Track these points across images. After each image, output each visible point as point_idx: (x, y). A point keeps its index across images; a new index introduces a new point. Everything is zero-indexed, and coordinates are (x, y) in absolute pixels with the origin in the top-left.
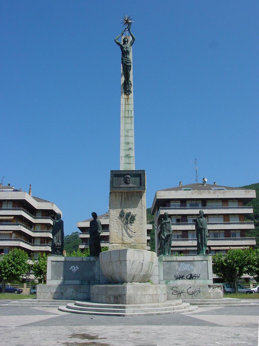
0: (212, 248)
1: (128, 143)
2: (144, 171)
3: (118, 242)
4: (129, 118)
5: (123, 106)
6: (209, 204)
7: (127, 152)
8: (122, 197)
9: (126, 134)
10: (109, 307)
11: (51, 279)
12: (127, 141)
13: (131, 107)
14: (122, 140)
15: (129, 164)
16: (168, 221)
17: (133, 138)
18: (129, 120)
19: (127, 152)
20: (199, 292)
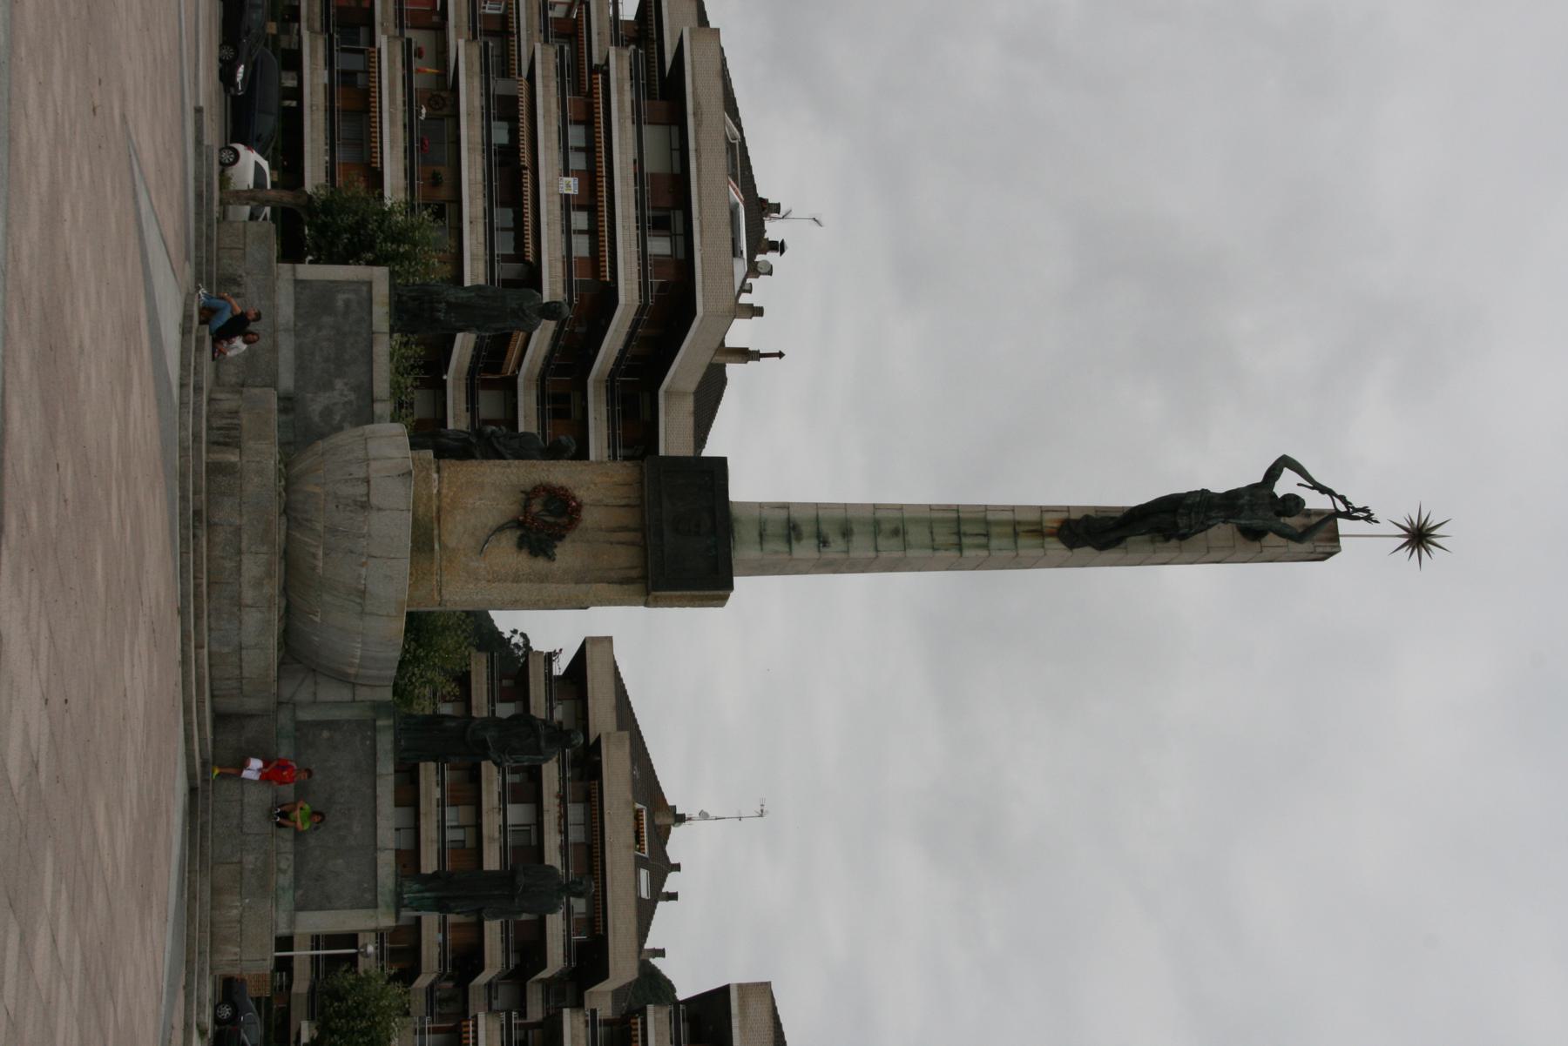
2: (610, 639)
3: (444, 491)
4: (954, 539)
11: (297, 282)
12: (856, 529)
15: (761, 536)
16: (543, 744)
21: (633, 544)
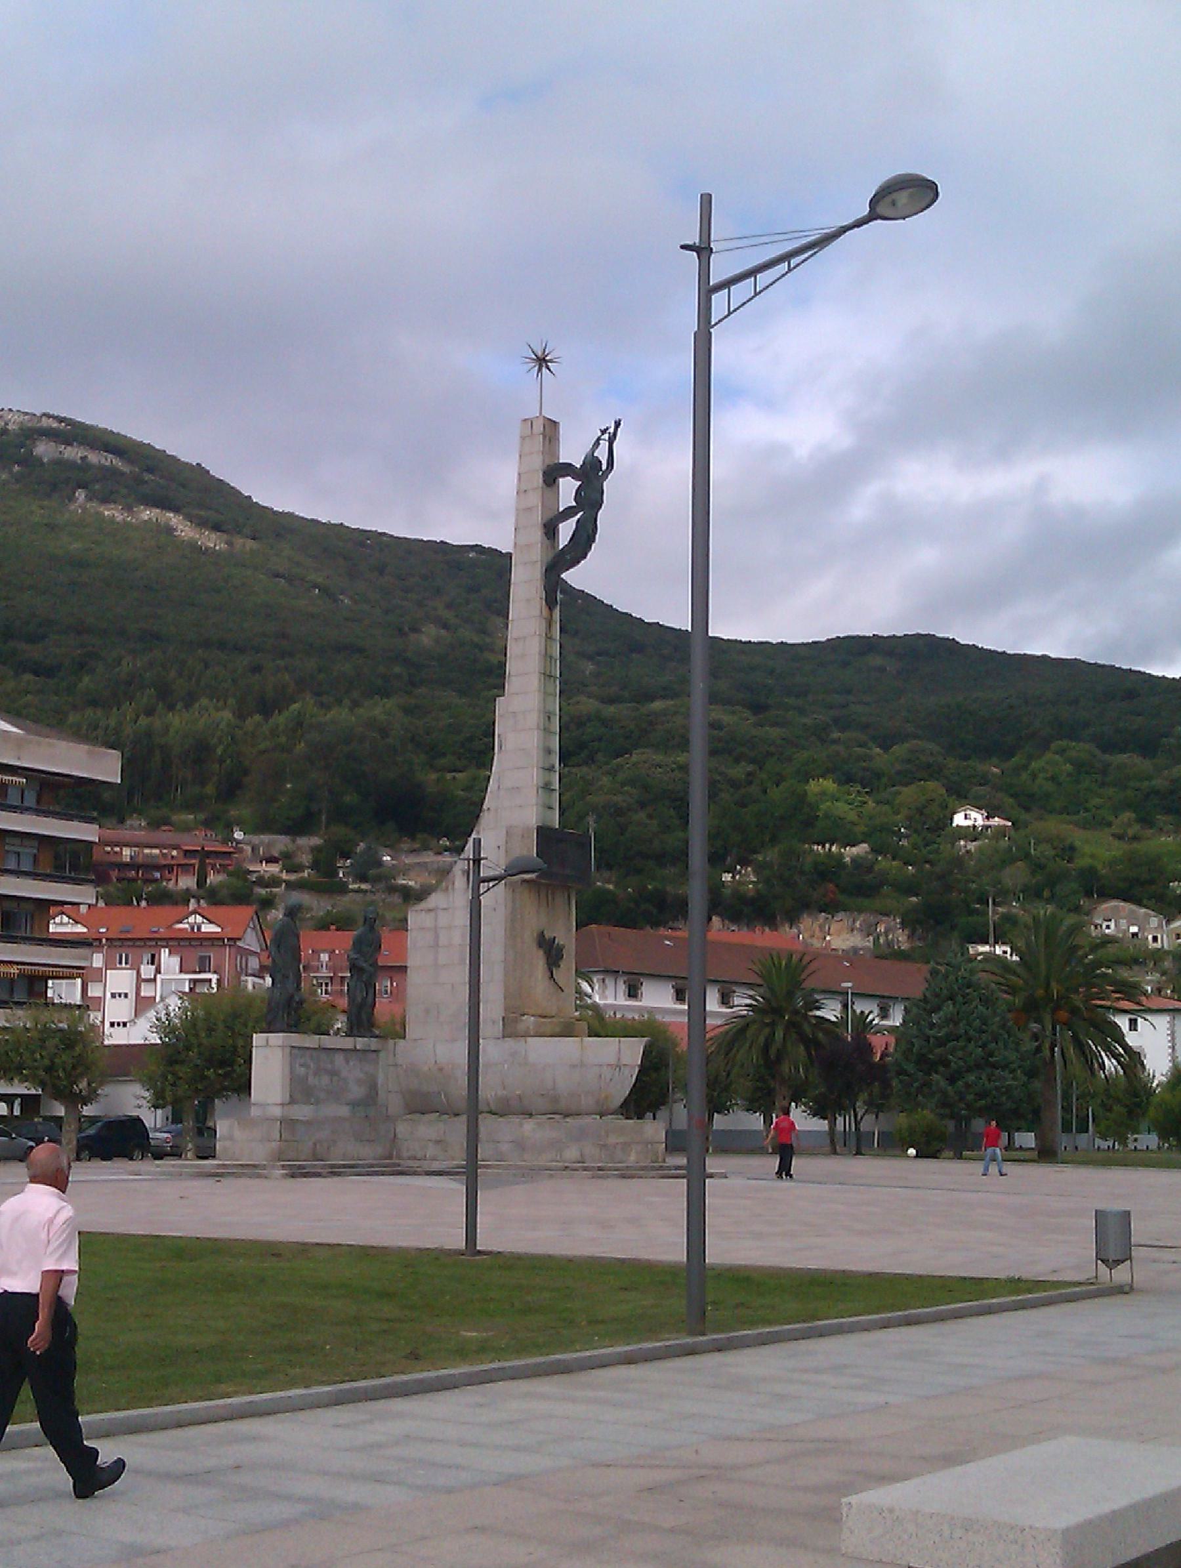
21: (553, 894)
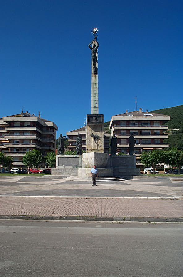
0: (143, 148)
1: (95, 100)
5: (93, 81)
6: (155, 124)
7: (95, 105)
8: (92, 127)
9: (94, 96)
10: (53, 219)
13: (97, 82)
14: (92, 99)
17: (98, 98)
18: (96, 89)
19: (95, 105)
20: (23, 107)
